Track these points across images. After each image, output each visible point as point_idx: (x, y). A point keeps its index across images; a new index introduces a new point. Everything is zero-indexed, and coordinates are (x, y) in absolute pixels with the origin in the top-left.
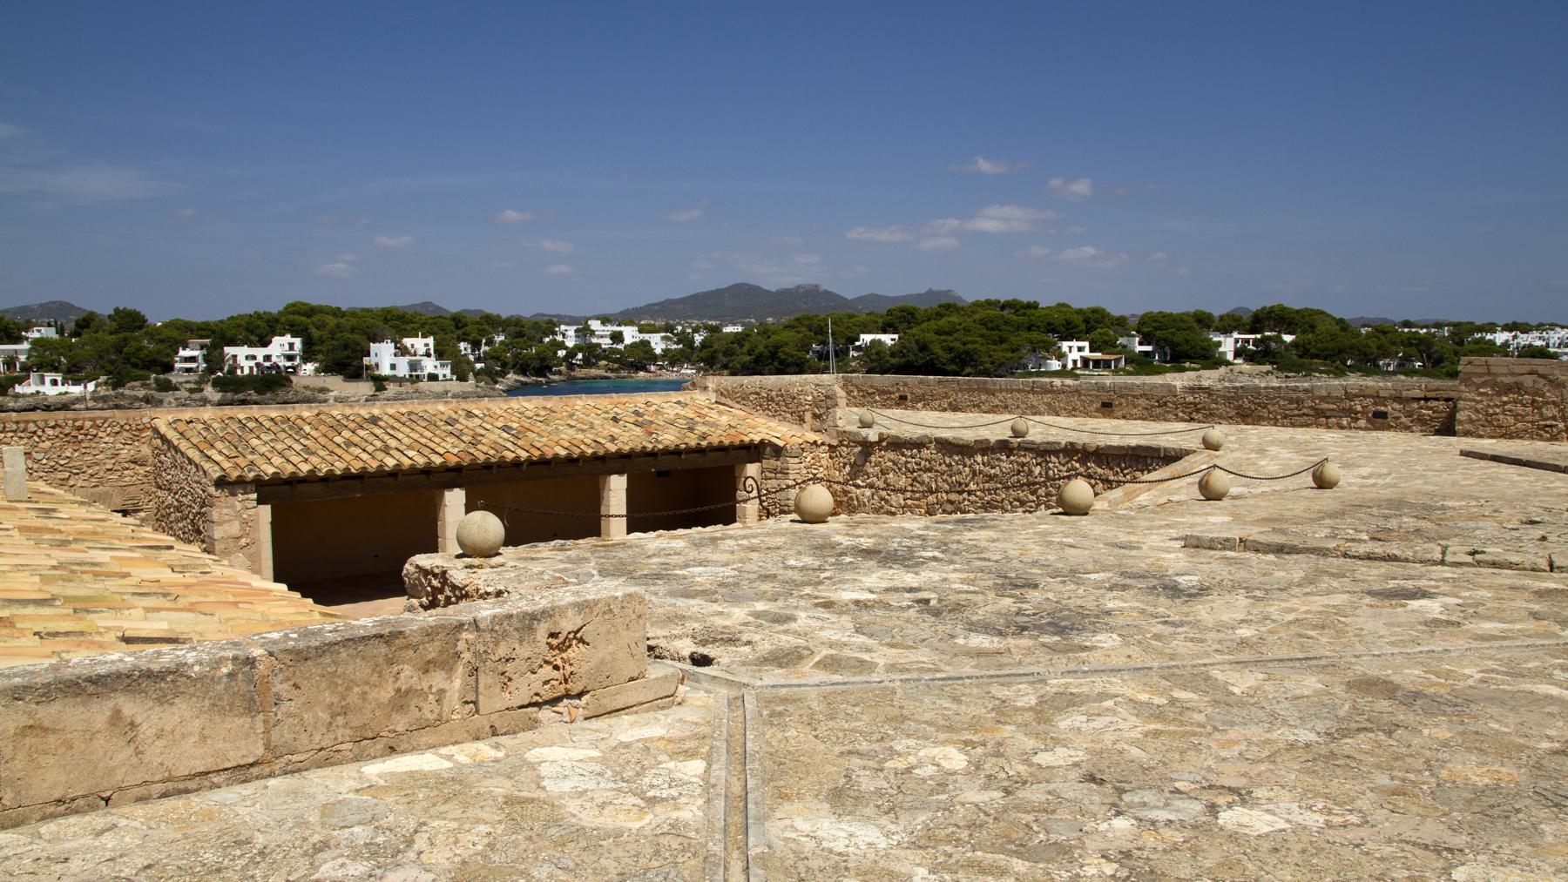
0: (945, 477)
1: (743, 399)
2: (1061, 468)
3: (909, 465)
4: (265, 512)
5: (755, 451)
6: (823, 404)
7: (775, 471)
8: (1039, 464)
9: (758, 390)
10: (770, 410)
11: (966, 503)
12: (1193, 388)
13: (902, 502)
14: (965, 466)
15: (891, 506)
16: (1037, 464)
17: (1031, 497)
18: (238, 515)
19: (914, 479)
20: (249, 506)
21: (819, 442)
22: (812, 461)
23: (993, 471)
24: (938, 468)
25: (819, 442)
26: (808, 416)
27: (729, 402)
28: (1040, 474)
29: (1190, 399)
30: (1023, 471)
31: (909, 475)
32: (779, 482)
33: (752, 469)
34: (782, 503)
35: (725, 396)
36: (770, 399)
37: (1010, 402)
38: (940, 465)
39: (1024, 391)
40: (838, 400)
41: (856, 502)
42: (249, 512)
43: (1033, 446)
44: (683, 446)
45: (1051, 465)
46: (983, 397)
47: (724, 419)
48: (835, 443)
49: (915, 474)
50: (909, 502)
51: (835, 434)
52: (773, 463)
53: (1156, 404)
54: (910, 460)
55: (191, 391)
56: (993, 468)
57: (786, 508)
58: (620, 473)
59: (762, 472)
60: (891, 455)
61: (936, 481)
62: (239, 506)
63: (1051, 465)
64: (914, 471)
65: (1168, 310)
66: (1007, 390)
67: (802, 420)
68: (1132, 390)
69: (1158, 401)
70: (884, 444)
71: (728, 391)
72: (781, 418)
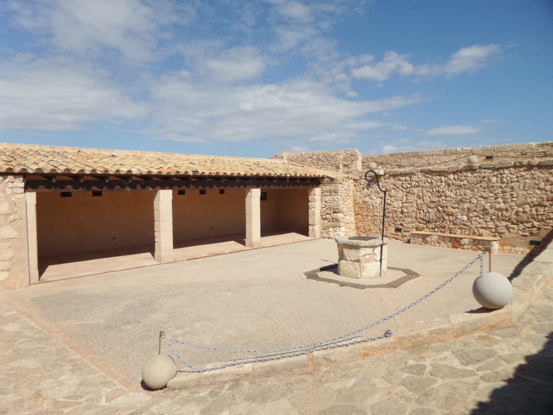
0: (428, 189)
1: (303, 161)
2: (512, 176)
3: (404, 185)
4: (32, 197)
5: (316, 181)
6: (349, 159)
7: (330, 191)
8: (496, 176)
9: (312, 156)
10: (319, 165)
11: (444, 202)
12: (543, 145)
13: (401, 205)
14: (441, 182)
15: (394, 207)
16: (494, 176)
17: (491, 195)
18: (7, 198)
19: (409, 192)
20: (18, 192)
21: (350, 178)
22: (347, 187)
23: (462, 183)
24: (424, 185)
25: (350, 178)
26: (341, 166)
27: (295, 163)
28: (497, 181)
29: (541, 150)
30: (484, 181)
31: (404, 190)
32: (332, 197)
33: (317, 191)
34: (335, 208)
35: (292, 161)
36: (319, 159)
37: (431, 161)
38: (425, 183)
39: (439, 155)
40: (358, 156)
41: (372, 207)
42: (17, 196)
43: (491, 166)
44: (288, 175)
45: (505, 176)
46: (416, 160)
47: (317, 152)
48: (357, 178)
49: (408, 190)
50: (405, 204)
51: (357, 174)
52: (328, 188)
53: (520, 154)
54: (404, 182)
55: (180, 312)
56: (461, 181)
57: (337, 211)
58: (257, 187)
59: (322, 193)
60: (392, 180)
61: (422, 192)
62: (9, 191)
63: (505, 176)
64: (407, 188)
65: (247, 233)
66: (430, 155)
67: (338, 168)
68: (505, 148)
69: (521, 153)
70: (387, 176)
71: (294, 158)
72: (325, 168)
